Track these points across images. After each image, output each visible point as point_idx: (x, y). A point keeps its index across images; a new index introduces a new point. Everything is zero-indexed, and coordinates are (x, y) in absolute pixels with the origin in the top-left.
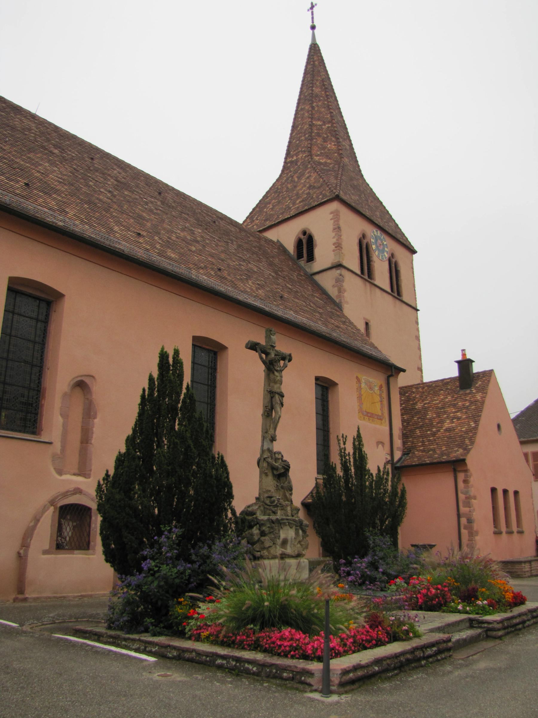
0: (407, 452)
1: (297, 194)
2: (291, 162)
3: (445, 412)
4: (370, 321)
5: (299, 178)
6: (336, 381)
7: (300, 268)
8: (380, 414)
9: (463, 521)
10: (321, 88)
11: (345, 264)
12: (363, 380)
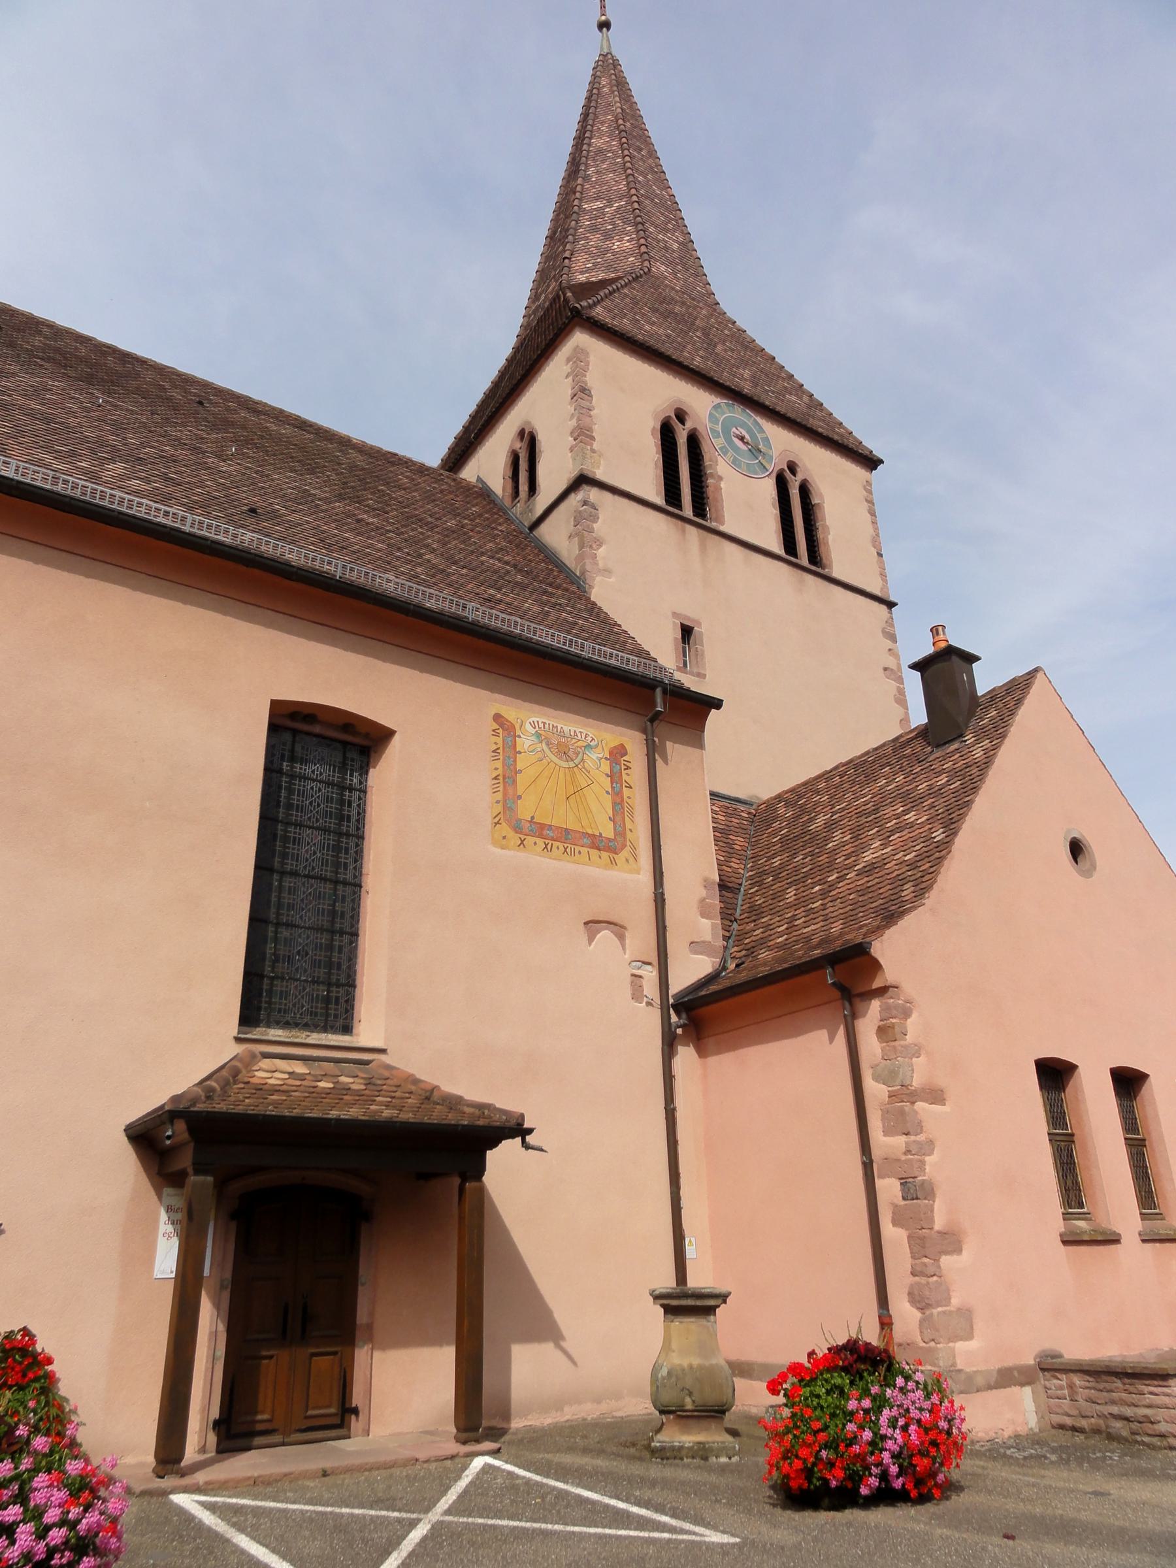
4: (699, 624)
6: (383, 719)
8: (608, 831)
9: (889, 1189)
10: (610, 136)
11: (600, 475)
12: (528, 727)
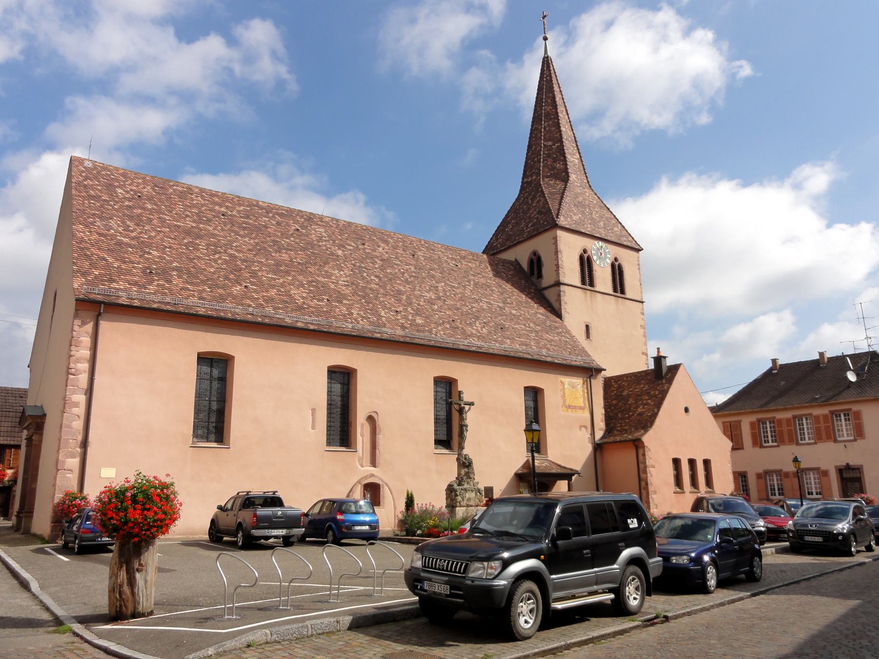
0: (609, 430)
1: (530, 217)
2: (527, 182)
3: (641, 400)
5: (532, 200)
7: (533, 284)
